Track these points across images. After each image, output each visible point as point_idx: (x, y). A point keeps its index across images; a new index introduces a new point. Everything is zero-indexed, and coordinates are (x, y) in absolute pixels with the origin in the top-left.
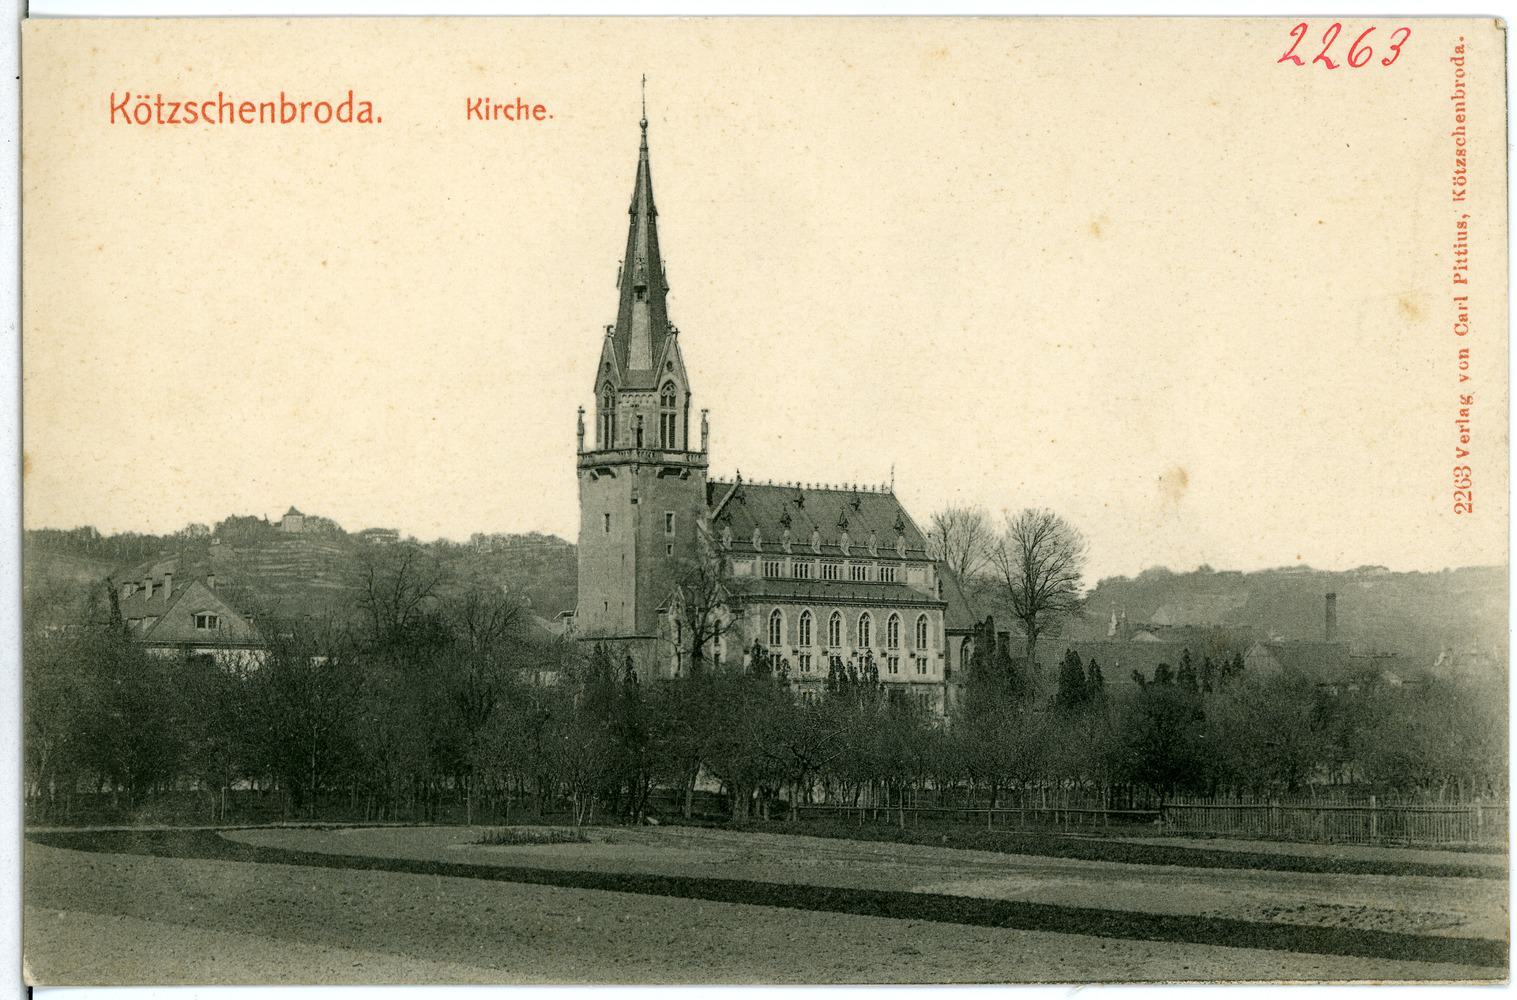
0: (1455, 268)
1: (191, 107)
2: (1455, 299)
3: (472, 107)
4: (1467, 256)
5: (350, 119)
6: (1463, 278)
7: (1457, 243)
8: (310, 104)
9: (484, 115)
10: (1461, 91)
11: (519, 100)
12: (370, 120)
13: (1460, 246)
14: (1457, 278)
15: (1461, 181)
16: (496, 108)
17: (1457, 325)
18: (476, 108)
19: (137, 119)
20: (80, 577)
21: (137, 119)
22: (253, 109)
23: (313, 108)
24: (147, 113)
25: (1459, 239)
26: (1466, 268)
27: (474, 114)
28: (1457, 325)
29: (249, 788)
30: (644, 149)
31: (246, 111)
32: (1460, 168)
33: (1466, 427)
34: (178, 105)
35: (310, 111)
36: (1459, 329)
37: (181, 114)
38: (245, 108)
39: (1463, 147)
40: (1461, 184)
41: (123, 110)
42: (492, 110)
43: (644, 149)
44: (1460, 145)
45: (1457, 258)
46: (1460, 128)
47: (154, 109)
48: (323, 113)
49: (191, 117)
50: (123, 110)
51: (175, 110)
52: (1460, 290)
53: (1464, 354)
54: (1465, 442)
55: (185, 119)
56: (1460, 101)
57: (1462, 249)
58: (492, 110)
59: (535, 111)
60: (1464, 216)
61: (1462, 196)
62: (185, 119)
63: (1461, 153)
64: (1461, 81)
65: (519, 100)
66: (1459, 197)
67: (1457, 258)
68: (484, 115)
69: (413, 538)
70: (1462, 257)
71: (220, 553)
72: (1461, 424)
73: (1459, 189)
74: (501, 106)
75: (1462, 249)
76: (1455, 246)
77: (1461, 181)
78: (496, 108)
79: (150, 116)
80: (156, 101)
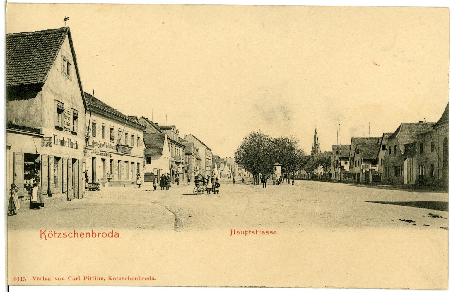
2: (79, 277)
3: (42, 233)
4: (92, 280)
5: (112, 237)
6: (86, 279)
7: (96, 278)
10: (141, 279)
12: (118, 237)
13: (96, 278)
14: (86, 277)
15: (114, 279)
17: (71, 277)
19: (69, 237)
22: (84, 234)
23: (101, 234)
25: (98, 278)
26: (89, 280)
28: (71, 277)
31: (82, 235)
32: (118, 279)
33: (77, 279)
36: (70, 278)
38: (81, 234)
39: (273, 233)
40: (113, 279)
41: (44, 234)
44: (274, 233)
45: (92, 277)
46: (141, 279)
47: (54, 234)
50: (44, 234)
52: (82, 278)
53: (63, 279)
54: (37, 279)
55: (63, 237)
56: (138, 279)
57: (94, 279)
60: (104, 280)
61: (110, 279)
62: (63, 237)
63: (123, 279)
64: (144, 279)
66: (110, 278)
67: (92, 277)
70: (92, 279)
72: (43, 278)
73: (112, 278)
74: (100, 234)
75: (94, 279)
76: (96, 277)
77: (114, 279)
79: (69, 235)
80: (54, 232)
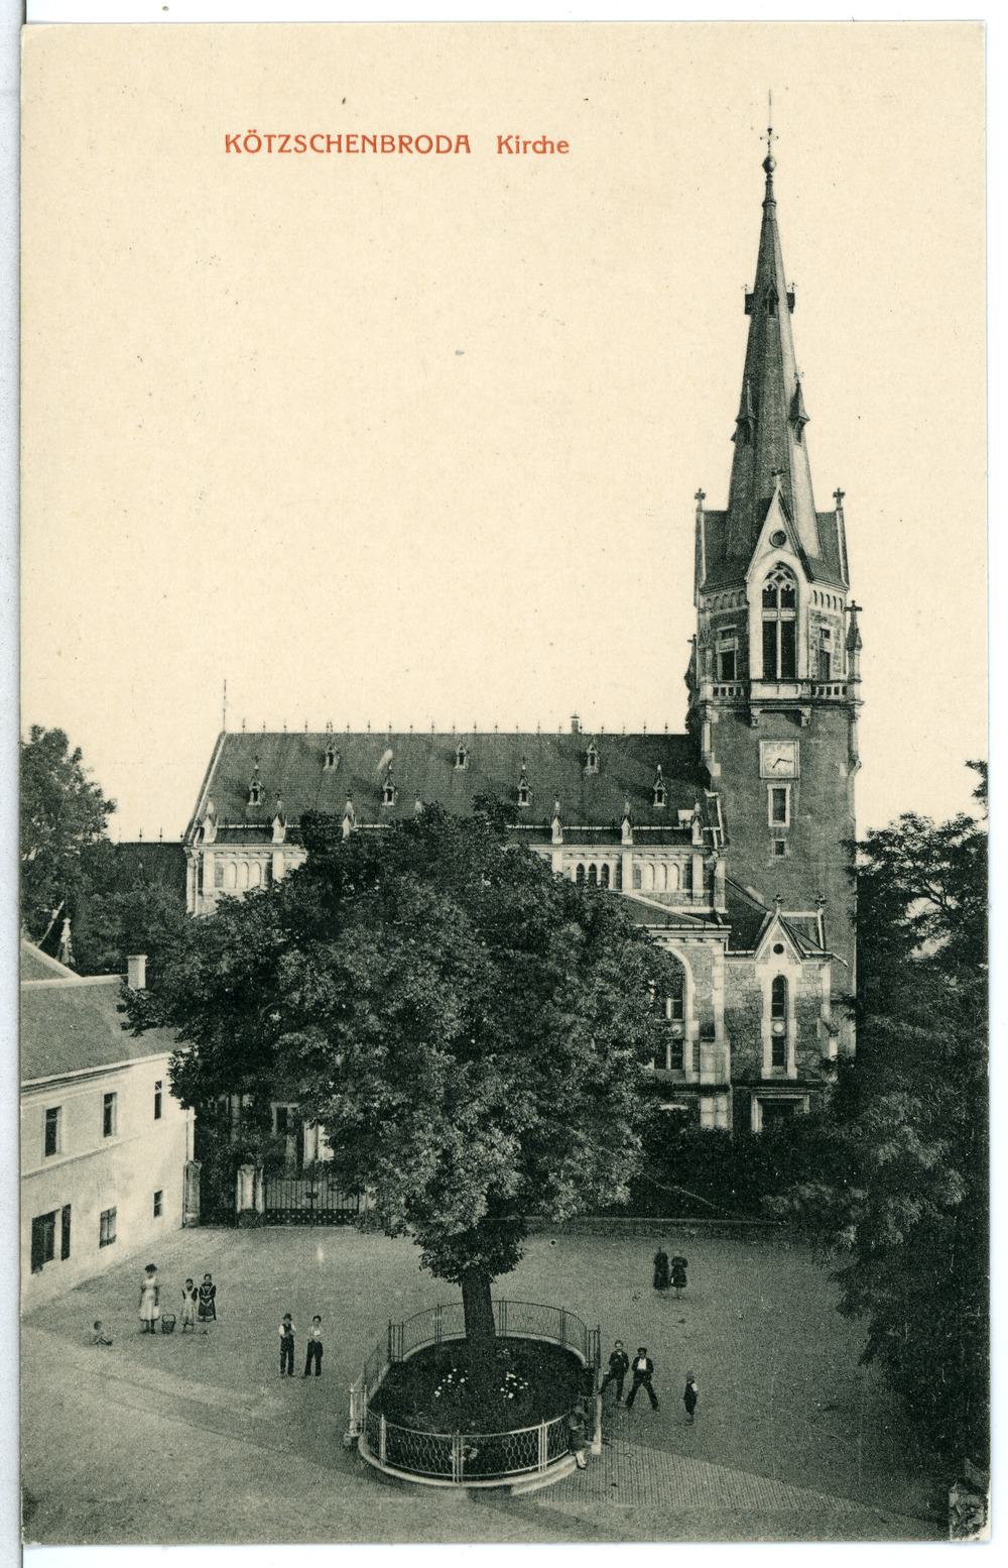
0: (518, 137)
1: (301, 139)
3: (502, 141)
8: (530, 142)
9: (514, 149)
11: (544, 137)
16: (525, 143)
18: (506, 142)
20: (586, 1509)
21: (246, 148)
24: (447, 142)
27: (504, 147)
29: (912, 865)
30: (768, 203)
34: (288, 137)
35: (529, 147)
37: (291, 144)
42: (521, 146)
43: (768, 203)
48: (444, 145)
49: (300, 148)
51: (285, 142)
58: (521, 146)
59: (559, 146)
62: (295, 149)
65: (544, 137)
68: (514, 149)
69: (733, 439)
71: (776, 991)
78: (525, 143)
